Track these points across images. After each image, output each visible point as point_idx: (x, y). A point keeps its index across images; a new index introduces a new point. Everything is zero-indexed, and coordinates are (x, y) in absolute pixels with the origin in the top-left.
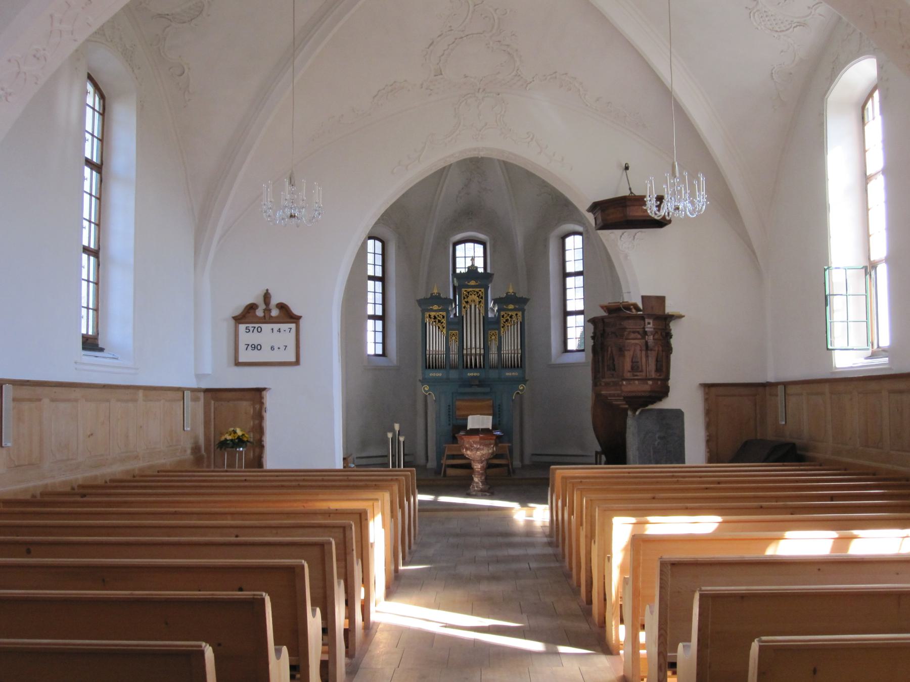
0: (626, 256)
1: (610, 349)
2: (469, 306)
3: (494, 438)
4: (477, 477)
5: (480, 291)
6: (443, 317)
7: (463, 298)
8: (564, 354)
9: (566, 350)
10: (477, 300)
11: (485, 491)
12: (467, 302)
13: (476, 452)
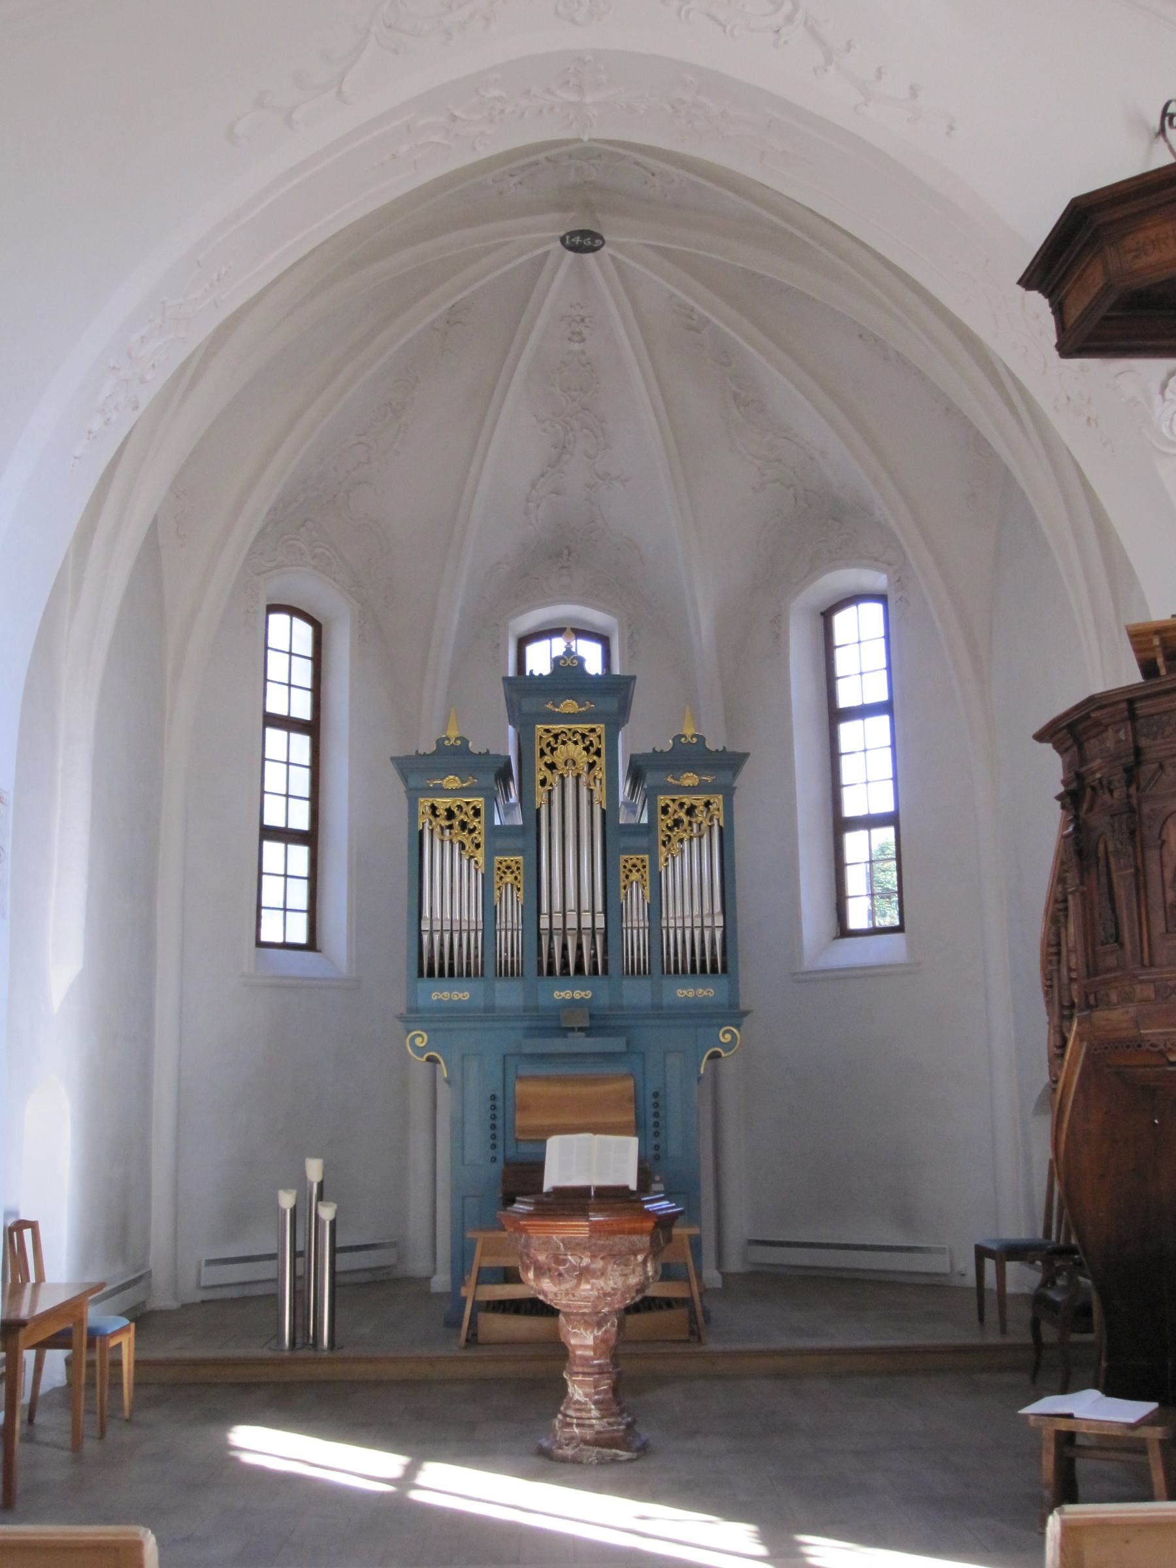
2: (557, 778)
3: (649, 1225)
4: (581, 1384)
5: (593, 730)
6: (477, 813)
7: (538, 754)
8: (841, 941)
9: (844, 932)
10: (583, 759)
11: (611, 1443)
12: (552, 767)
13: (578, 1284)
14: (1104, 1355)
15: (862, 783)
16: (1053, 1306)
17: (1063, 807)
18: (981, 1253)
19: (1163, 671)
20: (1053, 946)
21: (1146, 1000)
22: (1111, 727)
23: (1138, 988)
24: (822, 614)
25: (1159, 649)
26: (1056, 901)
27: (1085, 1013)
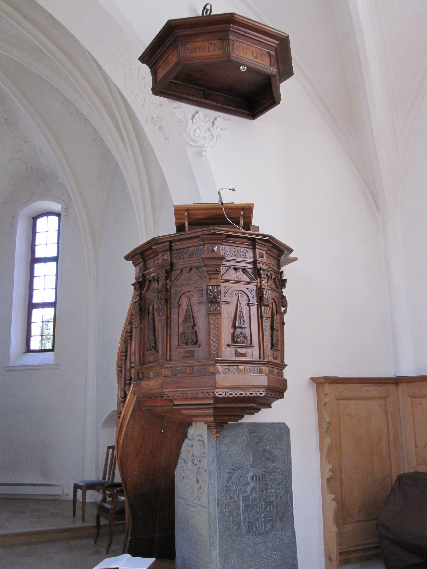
0: (200, 153)
1: (184, 302)
9: (28, 350)
14: (129, 535)
15: (41, 322)
16: (107, 510)
17: (135, 289)
18: (76, 487)
19: (187, 229)
20: (123, 352)
21: (167, 376)
22: (161, 253)
23: (163, 370)
24: (32, 218)
25: (187, 218)
26: (127, 332)
27: (138, 382)
